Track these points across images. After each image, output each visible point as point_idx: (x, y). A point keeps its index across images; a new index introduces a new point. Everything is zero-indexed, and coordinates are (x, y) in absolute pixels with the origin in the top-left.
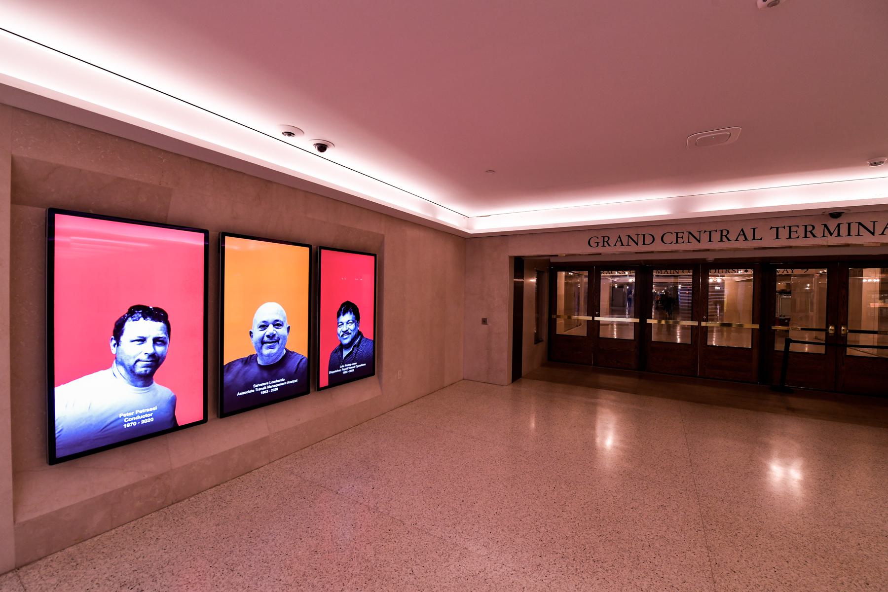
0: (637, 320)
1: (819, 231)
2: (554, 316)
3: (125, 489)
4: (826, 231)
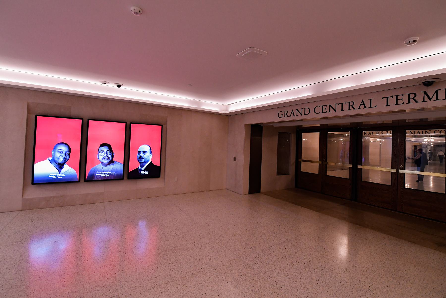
0: (359, 167)
1: (419, 98)
2: (300, 160)
3: (51, 197)
4: (426, 97)
